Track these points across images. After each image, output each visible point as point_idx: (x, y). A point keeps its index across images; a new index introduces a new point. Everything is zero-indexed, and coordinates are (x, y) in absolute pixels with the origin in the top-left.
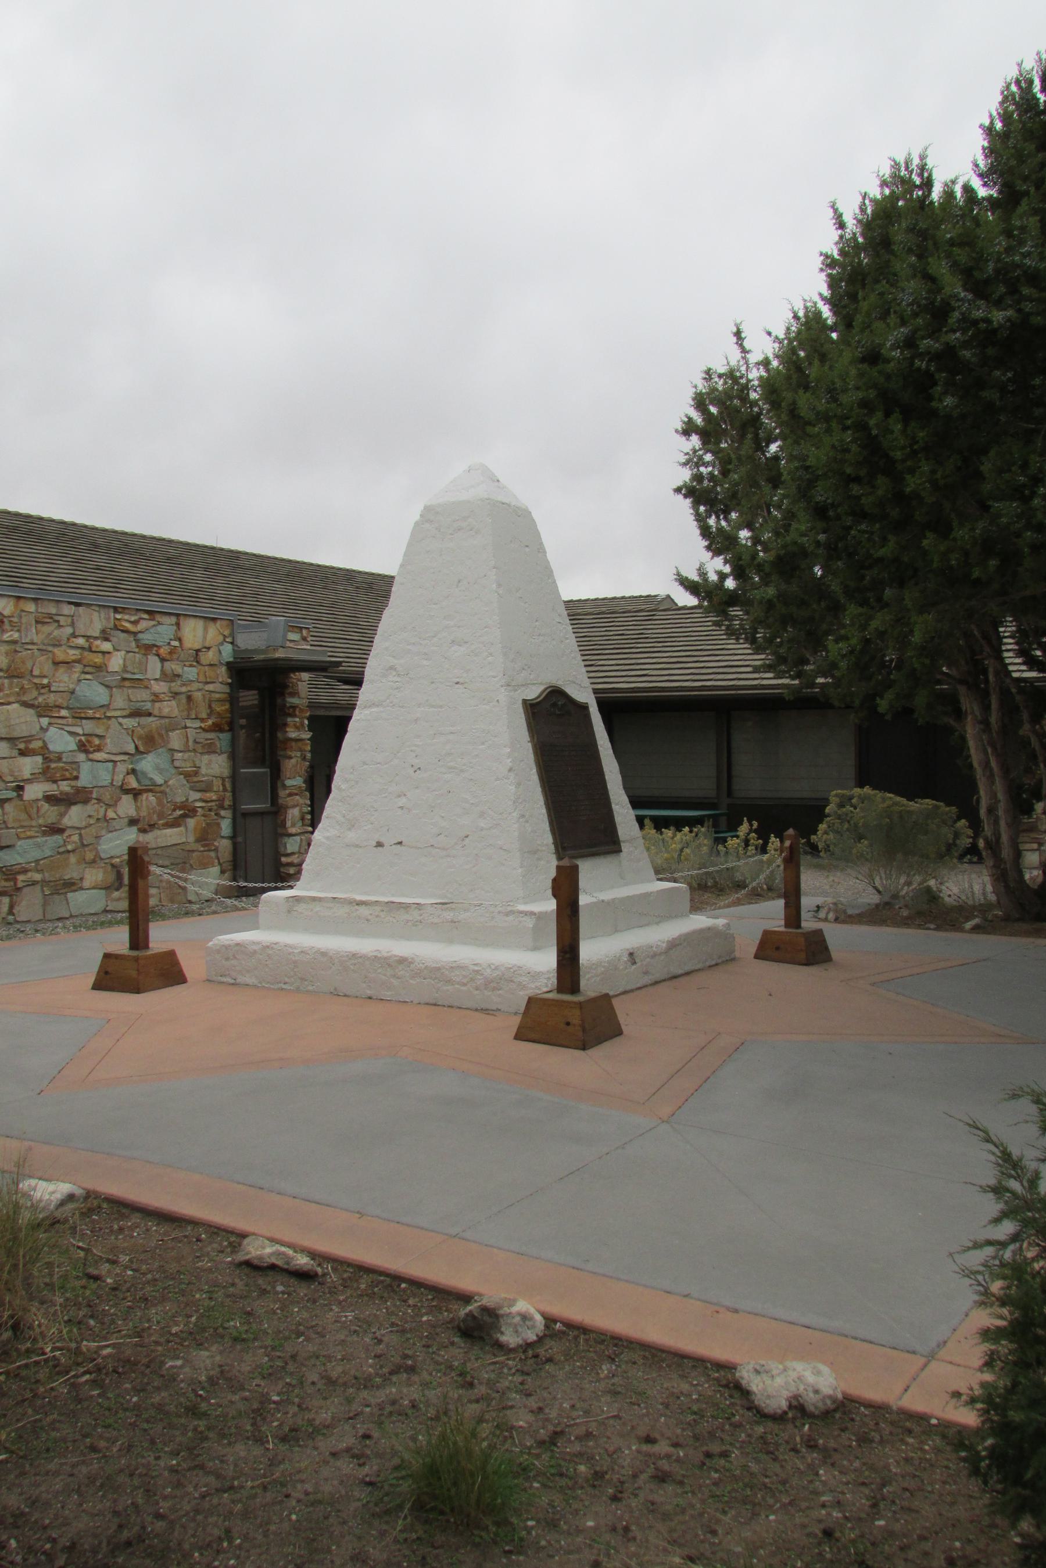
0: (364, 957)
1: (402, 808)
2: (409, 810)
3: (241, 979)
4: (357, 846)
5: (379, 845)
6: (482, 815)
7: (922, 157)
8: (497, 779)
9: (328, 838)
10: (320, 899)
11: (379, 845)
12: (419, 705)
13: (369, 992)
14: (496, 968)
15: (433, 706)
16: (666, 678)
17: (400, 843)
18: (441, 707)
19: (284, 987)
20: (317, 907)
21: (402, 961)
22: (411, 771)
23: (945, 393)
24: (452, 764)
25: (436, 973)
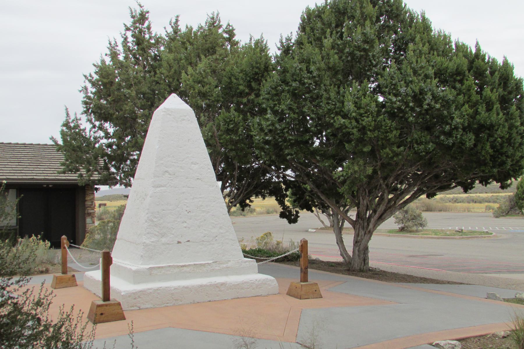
0: (206, 286)
1: (186, 227)
2: (189, 228)
3: (142, 306)
4: (168, 244)
5: (179, 242)
6: (221, 228)
7: (218, 15)
8: (224, 215)
9: (152, 242)
10: (162, 267)
11: (179, 242)
12: (184, 187)
13: (209, 299)
14: (259, 280)
15: (189, 187)
16: (20, 172)
17: (189, 241)
18: (193, 188)
19: (168, 305)
20: (185, 268)
21: (222, 284)
22: (186, 213)
23: (446, 126)
24: (204, 209)
25: (237, 286)
